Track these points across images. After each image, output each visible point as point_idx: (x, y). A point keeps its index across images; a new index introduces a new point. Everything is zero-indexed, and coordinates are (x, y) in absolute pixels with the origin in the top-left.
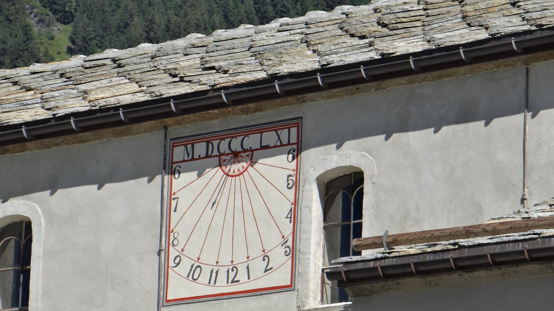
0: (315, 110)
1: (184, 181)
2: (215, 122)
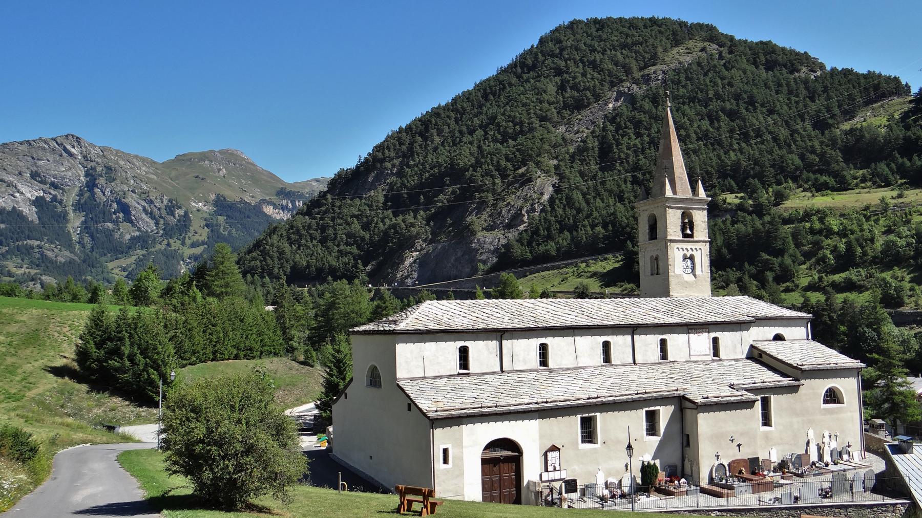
0: (710, 327)
1: (691, 335)
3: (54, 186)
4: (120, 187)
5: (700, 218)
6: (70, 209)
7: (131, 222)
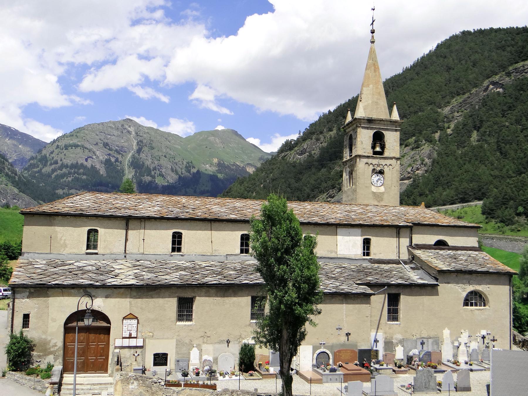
3: (118, 152)
4: (156, 153)
5: (392, 139)
6: (126, 167)
7: (163, 176)
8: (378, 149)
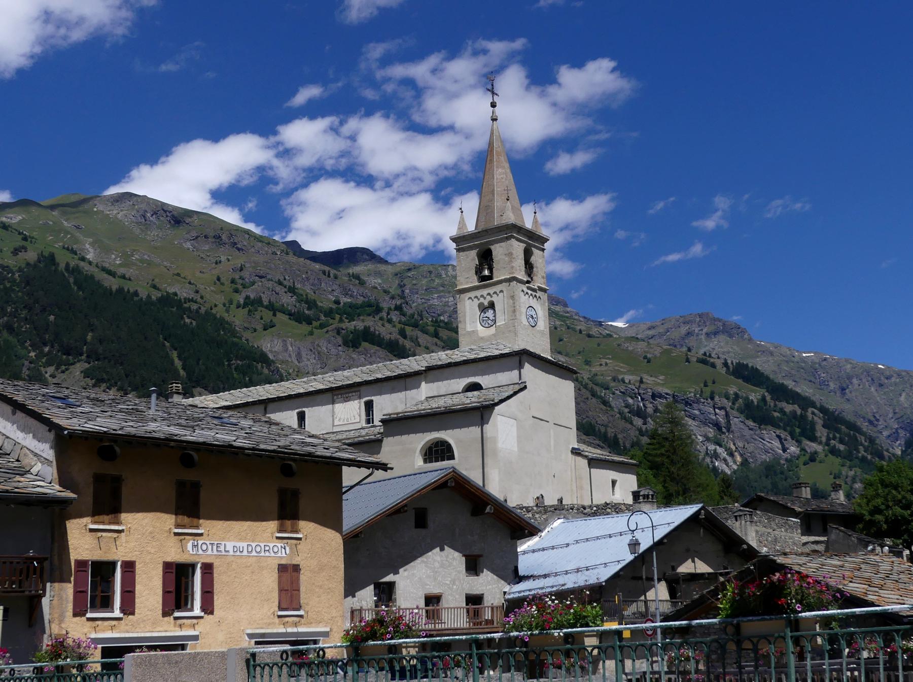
2: (343, 391)
8: (486, 273)
